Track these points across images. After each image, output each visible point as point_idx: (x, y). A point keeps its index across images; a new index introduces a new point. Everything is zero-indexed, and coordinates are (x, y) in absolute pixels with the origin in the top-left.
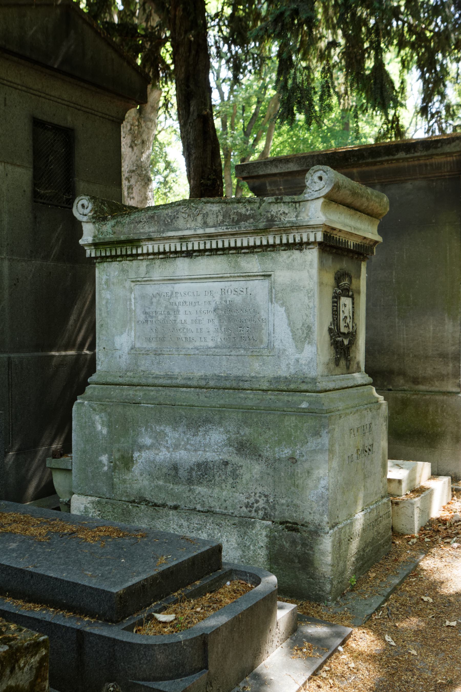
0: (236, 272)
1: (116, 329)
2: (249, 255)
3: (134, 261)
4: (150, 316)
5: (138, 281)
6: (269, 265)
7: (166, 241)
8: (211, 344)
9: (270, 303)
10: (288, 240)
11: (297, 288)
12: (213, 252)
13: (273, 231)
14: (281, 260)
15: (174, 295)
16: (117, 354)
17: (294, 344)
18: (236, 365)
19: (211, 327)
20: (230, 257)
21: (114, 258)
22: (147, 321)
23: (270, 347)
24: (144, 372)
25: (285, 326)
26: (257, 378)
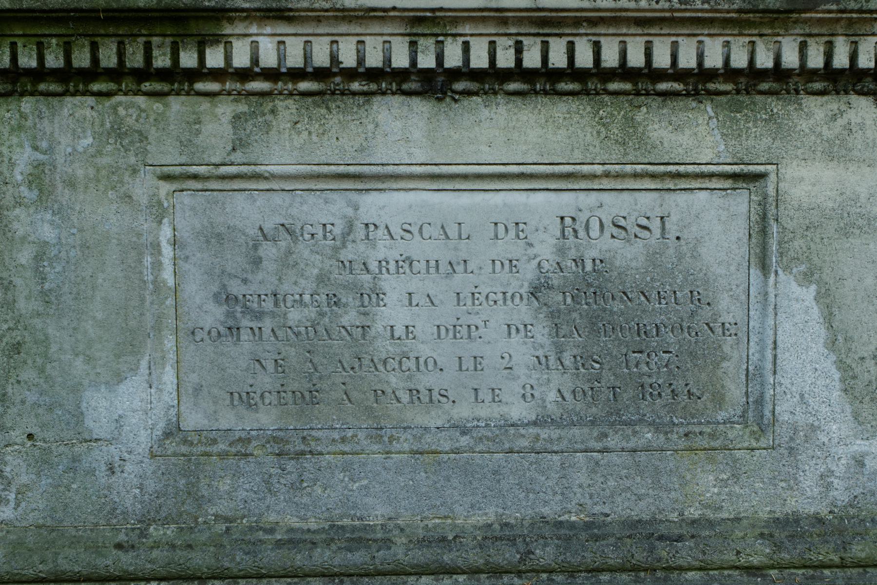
0: (631, 158)
1: (89, 360)
2: (681, 103)
3: (171, 99)
4: (247, 310)
5: (195, 177)
6: (757, 143)
7: (343, 28)
8: (518, 411)
9: (755, 273)
10: (853, 57)
11: (861, 222)
12: (542, 82)
13: (806, 21)
14: (804, 125)
15: (360, 233)
16: (99, 456)
17: (848, 409)
18: (628, 483)
19: (521, 352)
20: (603, 105)
21: (73, 80)
22: (234, 330)
23: (758, 416)
24: (227, 520)
25: (818, 348)
26: (711, 524)
